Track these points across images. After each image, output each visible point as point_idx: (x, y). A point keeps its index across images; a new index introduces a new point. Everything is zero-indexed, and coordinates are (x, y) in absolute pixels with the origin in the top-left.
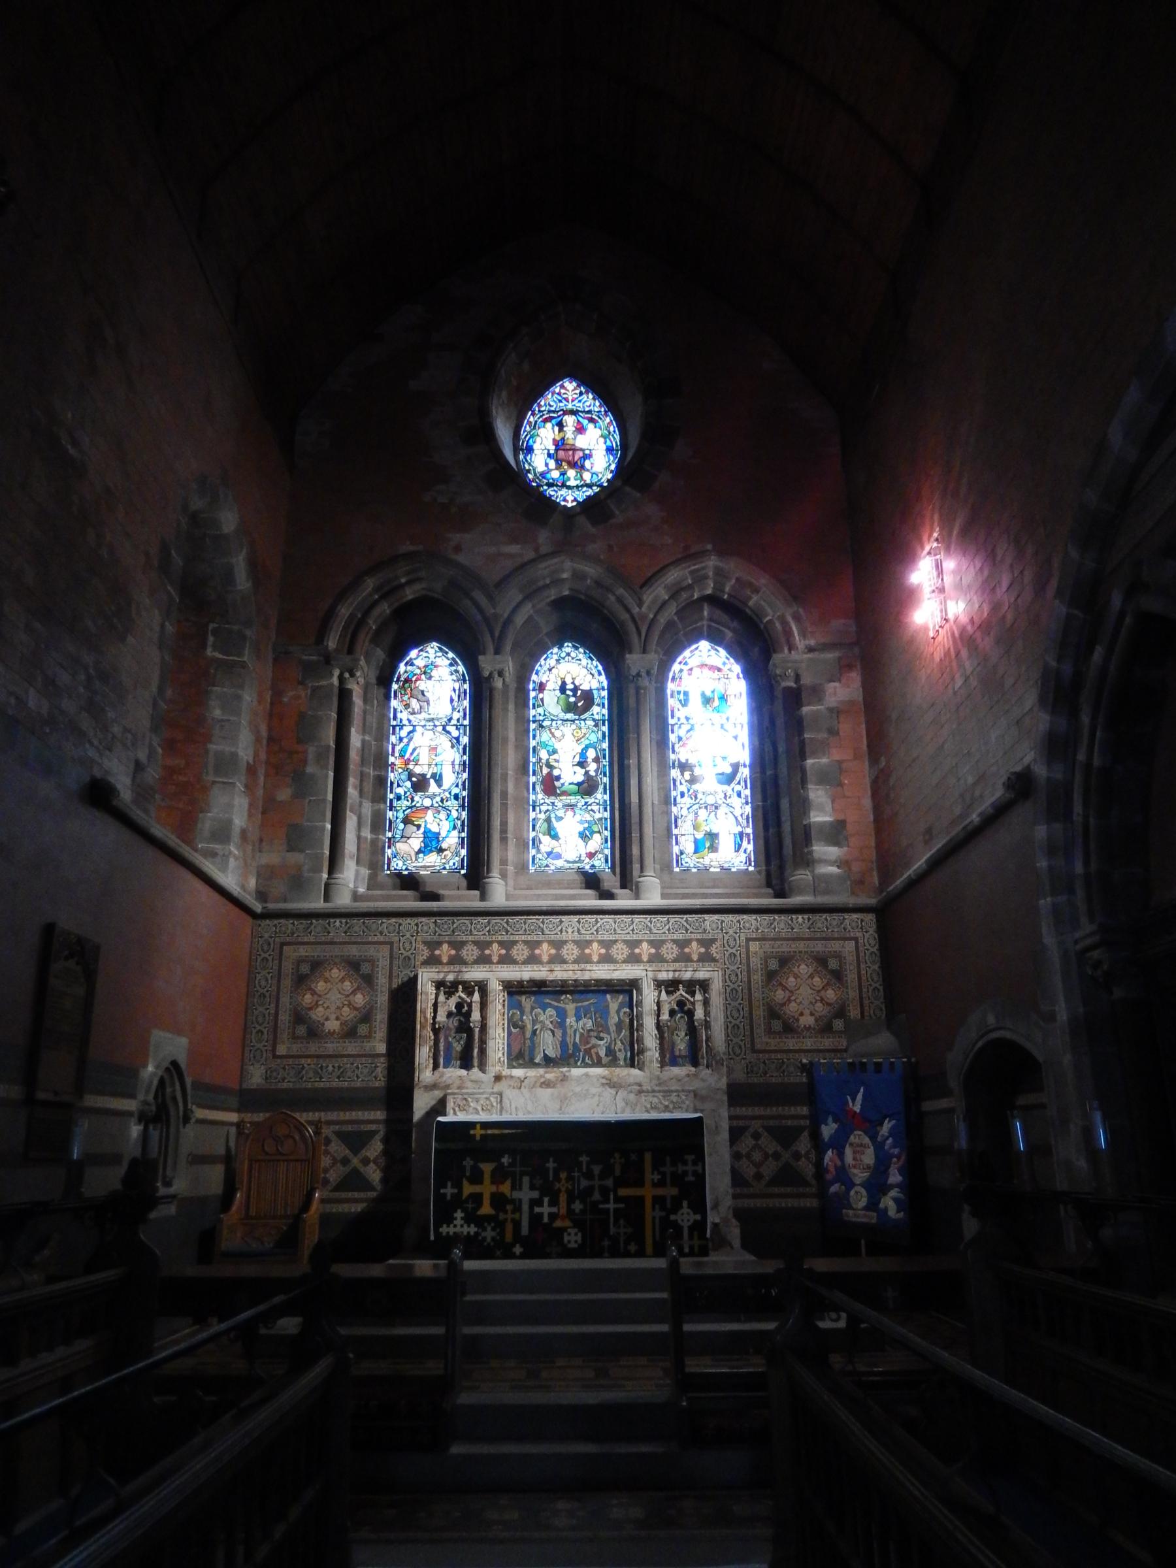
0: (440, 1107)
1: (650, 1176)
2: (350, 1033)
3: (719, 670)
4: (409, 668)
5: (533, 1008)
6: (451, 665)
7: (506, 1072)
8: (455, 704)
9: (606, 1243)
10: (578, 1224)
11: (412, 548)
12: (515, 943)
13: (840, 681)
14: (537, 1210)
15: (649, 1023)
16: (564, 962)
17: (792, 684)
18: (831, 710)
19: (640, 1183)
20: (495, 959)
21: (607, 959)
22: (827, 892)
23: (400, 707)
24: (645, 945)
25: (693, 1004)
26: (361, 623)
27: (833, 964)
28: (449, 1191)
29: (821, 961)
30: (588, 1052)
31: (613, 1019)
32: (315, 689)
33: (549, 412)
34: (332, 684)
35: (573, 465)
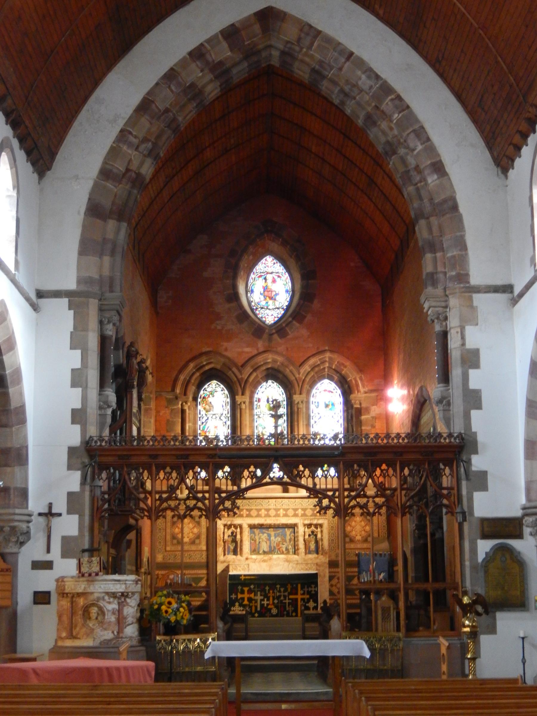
0: (227, 569)
1: (300, 592)
2: (193, 542)
3: (332, 392)
4: (205, 392)
5: (259, 534)
6: (222, 390)
7: (250, 556)
8: (224, 407)
9: (285, 613)
10: (276, 607)
11: (208, 349)
12: (252, 509)
13: (377, 405)
14: (262, 602)
15: (301, 539)
16: (270, 516)
17: (359, 406)
18: (373, 417)
19: (296, 594)
20: (245, 515)
21: (286, 515)
23: (202, 409)
24: (300, 510)
25: (317, 532)
26: (189, 382)
28: (233, 596)
30: (279, 549)
31: (288, 538)
32: (172, 410)
33: (261, 273)
34: (179, 408)
35: (271, 298)
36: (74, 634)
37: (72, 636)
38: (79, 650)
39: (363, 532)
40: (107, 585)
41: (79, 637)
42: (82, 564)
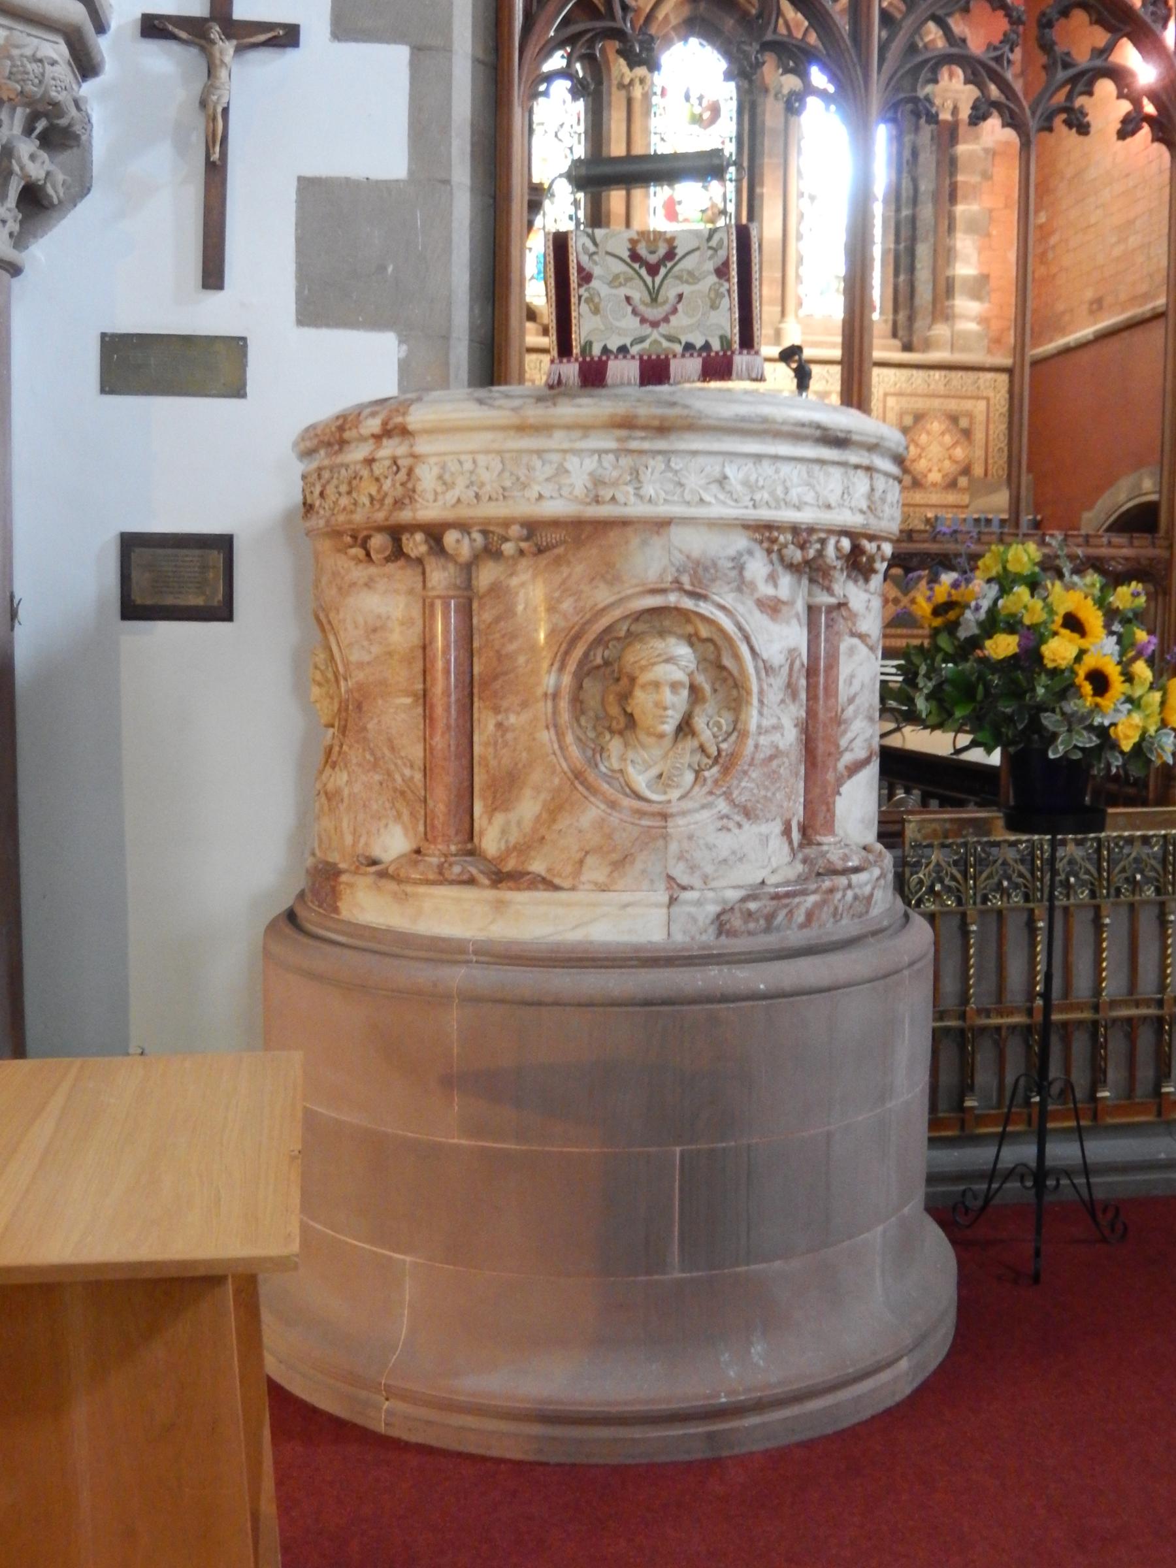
18: (986, 150)
22: (964, 349)
27: (964, 423)
29: (954, 419)
36: (491, 842)
37: (459, 854)
38: (563, 982)
39: (947, 463)
40: (767, 468)
41: (537, 866)
42: (586, 277)
